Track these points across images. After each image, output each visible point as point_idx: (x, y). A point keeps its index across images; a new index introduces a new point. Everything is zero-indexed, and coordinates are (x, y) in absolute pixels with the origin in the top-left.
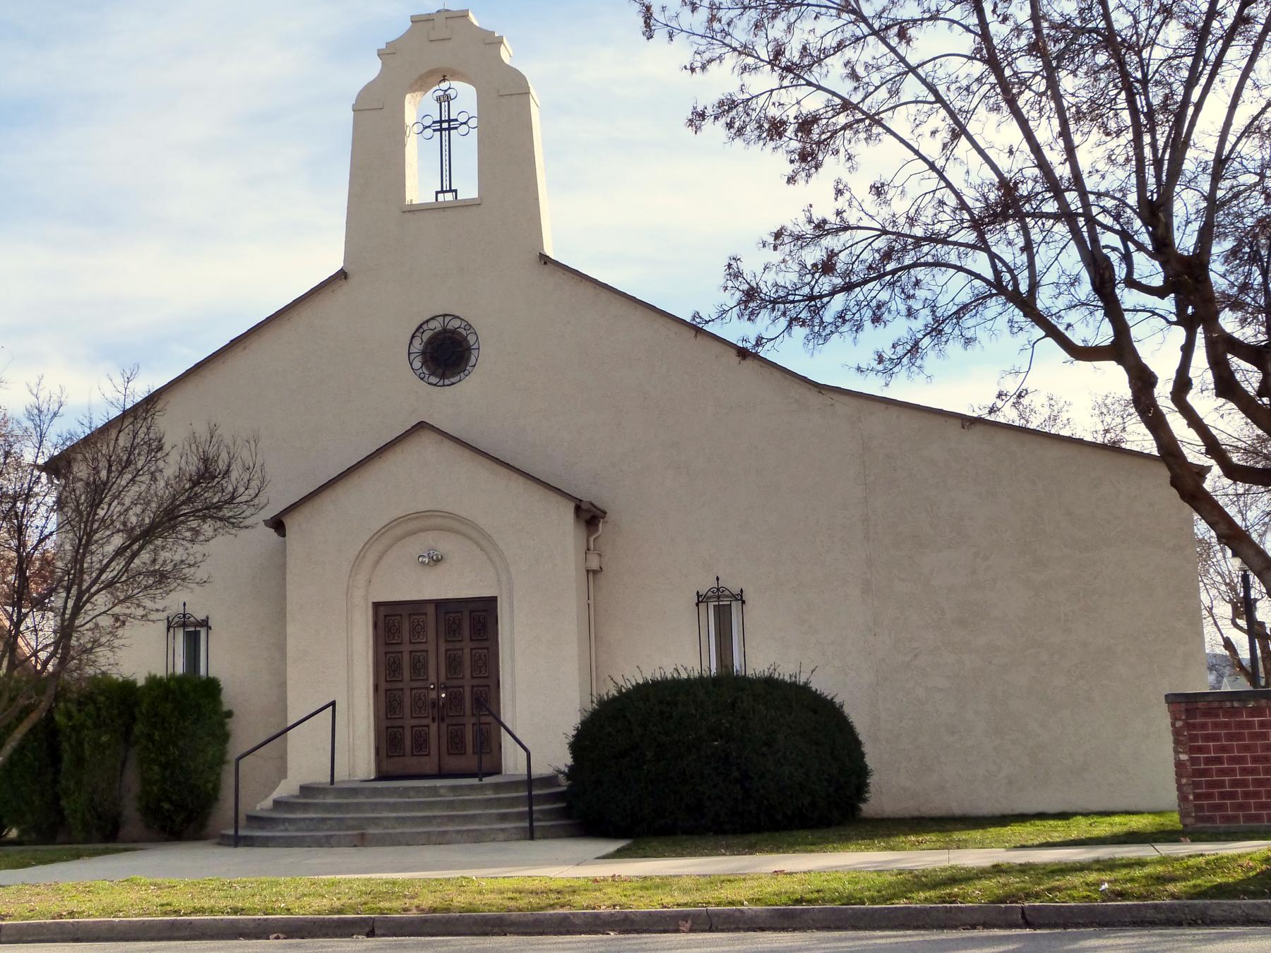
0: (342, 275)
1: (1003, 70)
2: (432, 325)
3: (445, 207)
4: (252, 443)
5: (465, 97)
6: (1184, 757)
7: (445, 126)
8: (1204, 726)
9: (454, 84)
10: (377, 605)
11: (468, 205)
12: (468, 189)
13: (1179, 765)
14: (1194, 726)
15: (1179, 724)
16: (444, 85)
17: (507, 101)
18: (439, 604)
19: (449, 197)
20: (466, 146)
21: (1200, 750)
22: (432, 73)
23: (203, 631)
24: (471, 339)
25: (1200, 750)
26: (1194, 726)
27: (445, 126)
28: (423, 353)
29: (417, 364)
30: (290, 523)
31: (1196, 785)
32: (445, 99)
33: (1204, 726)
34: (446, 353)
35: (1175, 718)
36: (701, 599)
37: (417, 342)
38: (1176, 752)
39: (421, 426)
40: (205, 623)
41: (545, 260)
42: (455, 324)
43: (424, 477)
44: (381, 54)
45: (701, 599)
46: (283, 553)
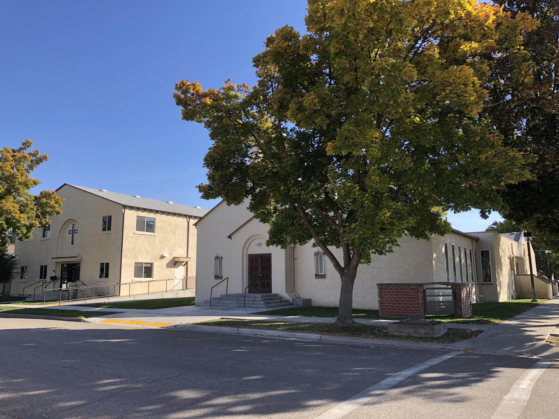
21: (383, 298)
25: (383, 298)
33: (384, 292)
40: (221, 258)
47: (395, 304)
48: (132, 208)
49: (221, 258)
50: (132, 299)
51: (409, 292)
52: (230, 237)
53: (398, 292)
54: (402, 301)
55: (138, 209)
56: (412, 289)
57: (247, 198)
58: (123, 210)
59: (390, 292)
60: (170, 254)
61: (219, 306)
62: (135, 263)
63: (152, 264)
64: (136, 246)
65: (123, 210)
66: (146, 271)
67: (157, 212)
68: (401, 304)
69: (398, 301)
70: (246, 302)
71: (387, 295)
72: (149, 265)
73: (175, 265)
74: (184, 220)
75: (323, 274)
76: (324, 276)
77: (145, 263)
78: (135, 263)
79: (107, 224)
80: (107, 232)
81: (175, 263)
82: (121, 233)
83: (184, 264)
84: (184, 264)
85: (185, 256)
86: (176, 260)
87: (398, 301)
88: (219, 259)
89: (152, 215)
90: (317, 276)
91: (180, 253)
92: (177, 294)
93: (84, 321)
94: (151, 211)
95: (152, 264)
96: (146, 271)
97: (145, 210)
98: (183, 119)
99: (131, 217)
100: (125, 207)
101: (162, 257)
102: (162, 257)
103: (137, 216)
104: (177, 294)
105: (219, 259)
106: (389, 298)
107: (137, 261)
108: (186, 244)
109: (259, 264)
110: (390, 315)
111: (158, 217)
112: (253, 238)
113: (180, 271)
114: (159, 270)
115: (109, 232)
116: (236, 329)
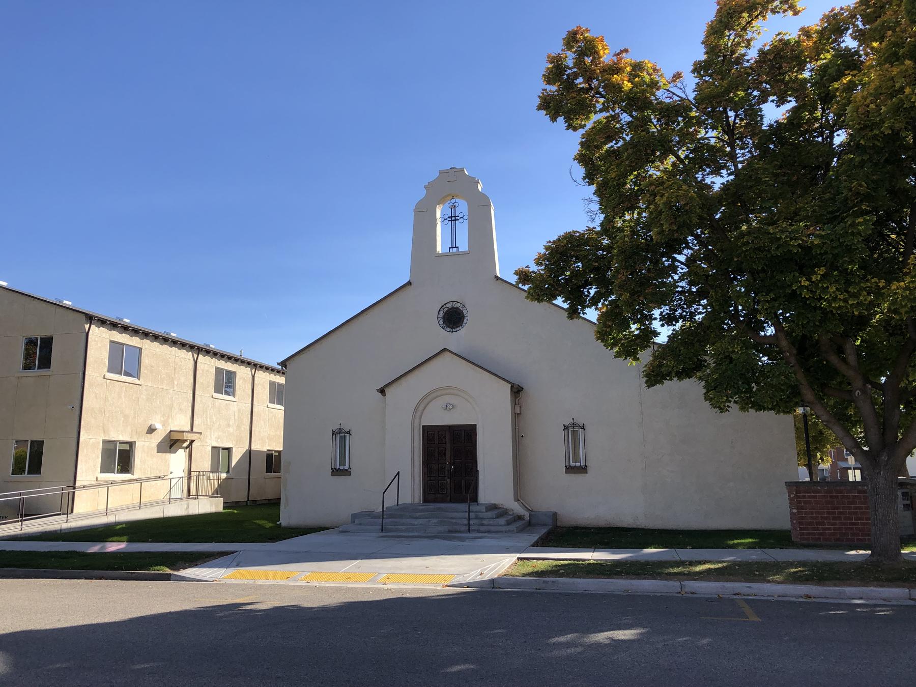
0: (409, 283)
1: (829, 171)
2: (448, 305)
3: (454, 255)
4: (193, 492)
5: (463, 208)
6: (795, 511)
7: (453, 219)
8: (804, 497)
9: (457, 200)
10: (425, 428)
11: (464, 254)
12: (463, 246)
13: (792, 514)
14: (799, 497)
15: (792, 496)
16: (453, 201)
17: (480, 209)
18: (450, 428)
19: (455, 250)
20: (462, 229)
21: (802, 508)
22: (448, 195)
23: (348, 436)
24: (465, 312)
25: (802, 508)
26: (799, 497)
27: (453, 219)
28: (444, 318)
29: (441, 322)
30: (387, 391)
31: (800, 523)
32: (453, 207)
33: (804, 497)
34: (453, 318)
35: (790, 493)
36: (566, 428)
37: (441, 313)
38: (791, 509)
39: (444, 350)
40: (349, 433)
41: (497, 278)
42: (458, 305)
43: (447, 371)
44: (426, 187)
45: (566, 428)
46: (384, 402)
47: (826, 518)
48: (102, 322)
49: (349, 433)
50: (111, 519)
51: (854, 497)
52: (382, 391)
53: (831, 497)
54: (841, 513)
55: (114, 326)
56: (859, 492)
57: (564, 302)
58: (87, 326)
59: (815, 497)
60: (164, 424)
61: (401, 531)
62: (104, 441)
63: (131, 444)
64: (109, 406)
65: (87, 326)
66: (121, 458)
67: (146, 335)
68: (840, 518)
69: (833, 513)
70: (466, 522)
71: (810, 503)
72: (126, 447)
73: (171, 447)
74: (187, 356)
75: (347, 467)
76: (583, 470)
77: (122, 443)
78: (104, 441)
79: (39, 353)
80: (36, 372)
81: (172, 443)
82: (81, 376)
83: (185, 445)
84: (185, 445)
85: (188, 428)
86: (176, 437)
87: (833, 513)
88: (341, 434)
89: (135, 341)
90: (570, 469)
91: (180, 423)
92: (187, 508)
93: (167, 578)
94: (135, 332)
95: (131, 444)
96: (121, 458)
97: (125, 329)
98: (539, 108)
99: (100, 340)
100: (90, 318)
101: (151, 430)
102: (151, 430)
103: (111, 342)
104: (187, 508)
105: (341, 434)
106: (813, 508)
107: (107, 438)
108: (190, 405)
109: (448, 445)
110: (838, 540)
111: (147, 345)
112: (452, 391)
113: (179, 458)
114: (146, 458)
115: (44, 372)
116: (677, 584)
